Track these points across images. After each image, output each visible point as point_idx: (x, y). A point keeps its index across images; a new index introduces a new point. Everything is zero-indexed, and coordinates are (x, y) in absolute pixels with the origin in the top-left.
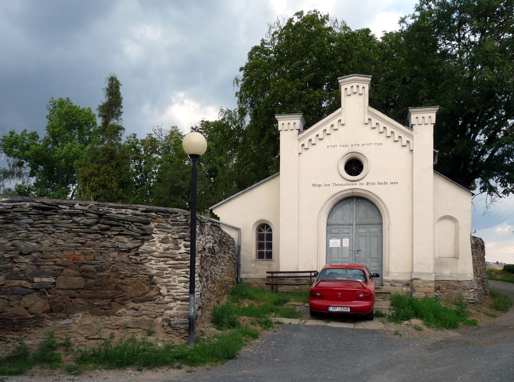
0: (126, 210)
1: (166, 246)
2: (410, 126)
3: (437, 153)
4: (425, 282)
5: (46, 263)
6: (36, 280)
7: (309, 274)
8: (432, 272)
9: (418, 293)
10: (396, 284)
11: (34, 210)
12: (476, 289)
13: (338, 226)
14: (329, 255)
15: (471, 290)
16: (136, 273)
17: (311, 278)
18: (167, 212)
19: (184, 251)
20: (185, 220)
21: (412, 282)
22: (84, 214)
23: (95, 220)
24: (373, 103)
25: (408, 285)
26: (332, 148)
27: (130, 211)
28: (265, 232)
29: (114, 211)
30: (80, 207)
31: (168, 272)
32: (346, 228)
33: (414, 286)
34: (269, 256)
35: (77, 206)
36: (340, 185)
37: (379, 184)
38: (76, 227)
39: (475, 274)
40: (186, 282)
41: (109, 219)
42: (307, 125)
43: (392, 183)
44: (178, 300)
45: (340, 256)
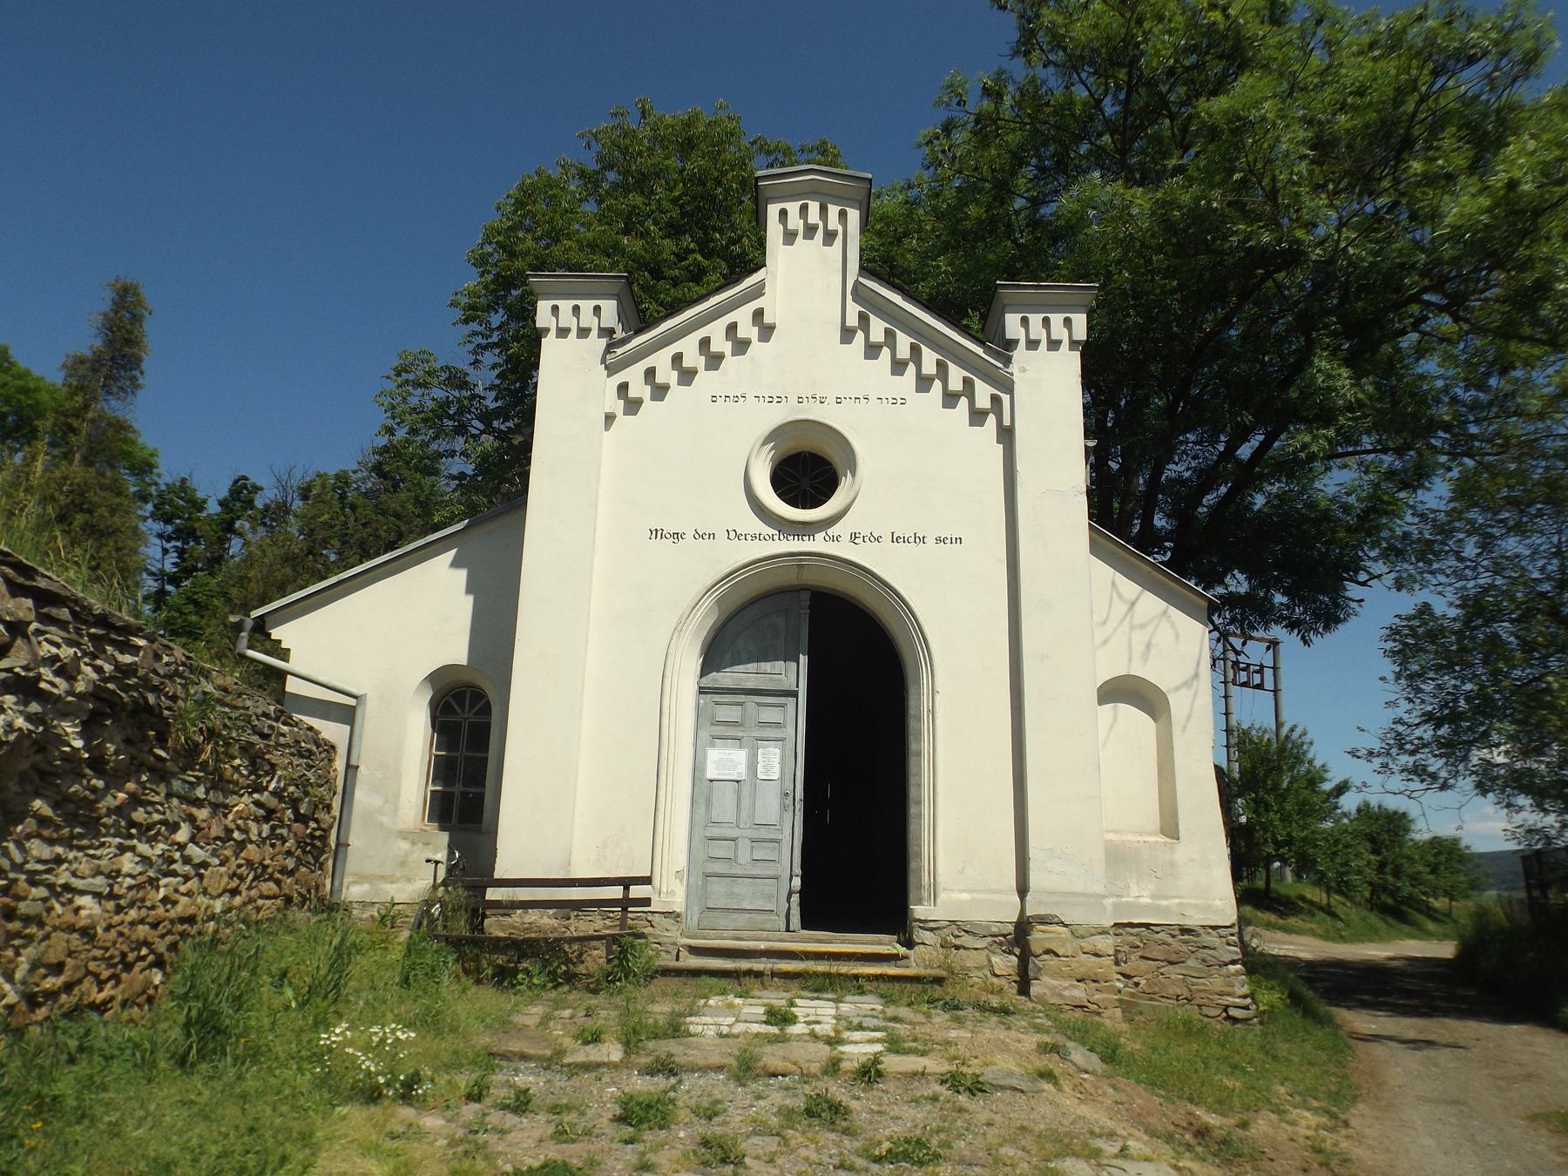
4: (1075, 932)
7: (616, 892)
9: (1055, 982)
10: (966, 940)
14: (701, 811)
17: (625, 909)
26: (730, 403)
36: (754, 537)
37: (895, 539)
42: (639, 318)
43: (938, 540)
45: (744, 816)
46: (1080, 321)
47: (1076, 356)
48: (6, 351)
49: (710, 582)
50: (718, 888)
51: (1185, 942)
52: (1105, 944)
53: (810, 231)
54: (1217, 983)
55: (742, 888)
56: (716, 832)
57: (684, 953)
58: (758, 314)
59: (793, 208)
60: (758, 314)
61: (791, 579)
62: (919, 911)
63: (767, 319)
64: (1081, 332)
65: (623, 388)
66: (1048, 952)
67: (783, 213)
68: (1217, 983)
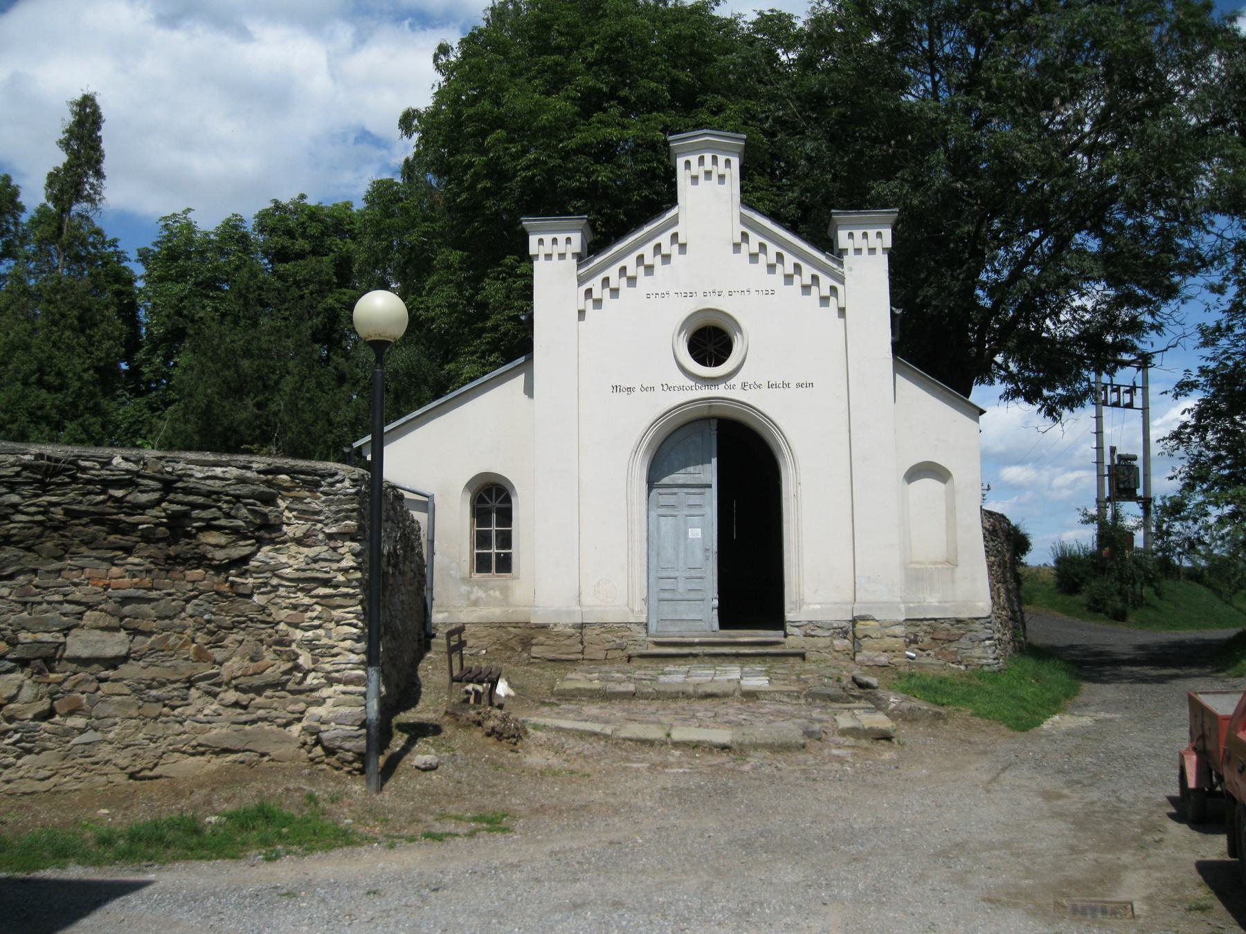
0: (224, 469)
1: (312, 552)
2: (836, 251)
3: (897, 315)
4: (884, 625)
5: (47, 598)
6: (24, 636)
8: (899, 600)
9: (870, 653)
10: (818, 632)
11: (25, 473)
12: (999, 639)
13: (675, 490)
15: (987, 642)
16: (243, 619)
18: (313, 472)
19: (352, 564)
20: (353, 491)
21: (854, 626)
22: (130, 481)
23: (156, 495)
24: (749, 198)
25: (843, 633)
27: (233, 472)
28: (495, 504)
29: (198, 472)
30: (125, 465)
31: (314, 614)
32: (694, 494)
33: (859, 635)
34: (505, 564)
35: (117, 461)
38: (115, 511)
39: (994, 603)
40: (358, 640)
41: (187, 491)
42: (596, 245)
43: (799, 385)
44: (339, 681)
46: (887, 233)
47: (886, 257)
48: (7, 179)
49: (652, 421)
50: (666, 607)
51: (960, 628)
52: (899, 630)
53: (708, 174)
54: (978, 652)
55: (682, 607)
56: (664, 574)
57: (651, 645)
58: (675, 237)
59: (694, 159)
60: (675, 237)
61: (705, 413)
62: (789, 616)
63: (681, 240)
64: (887, 240)
65: (589, 292)
66: (866, 636)
67: (688, 163)
68: (978, 652)
